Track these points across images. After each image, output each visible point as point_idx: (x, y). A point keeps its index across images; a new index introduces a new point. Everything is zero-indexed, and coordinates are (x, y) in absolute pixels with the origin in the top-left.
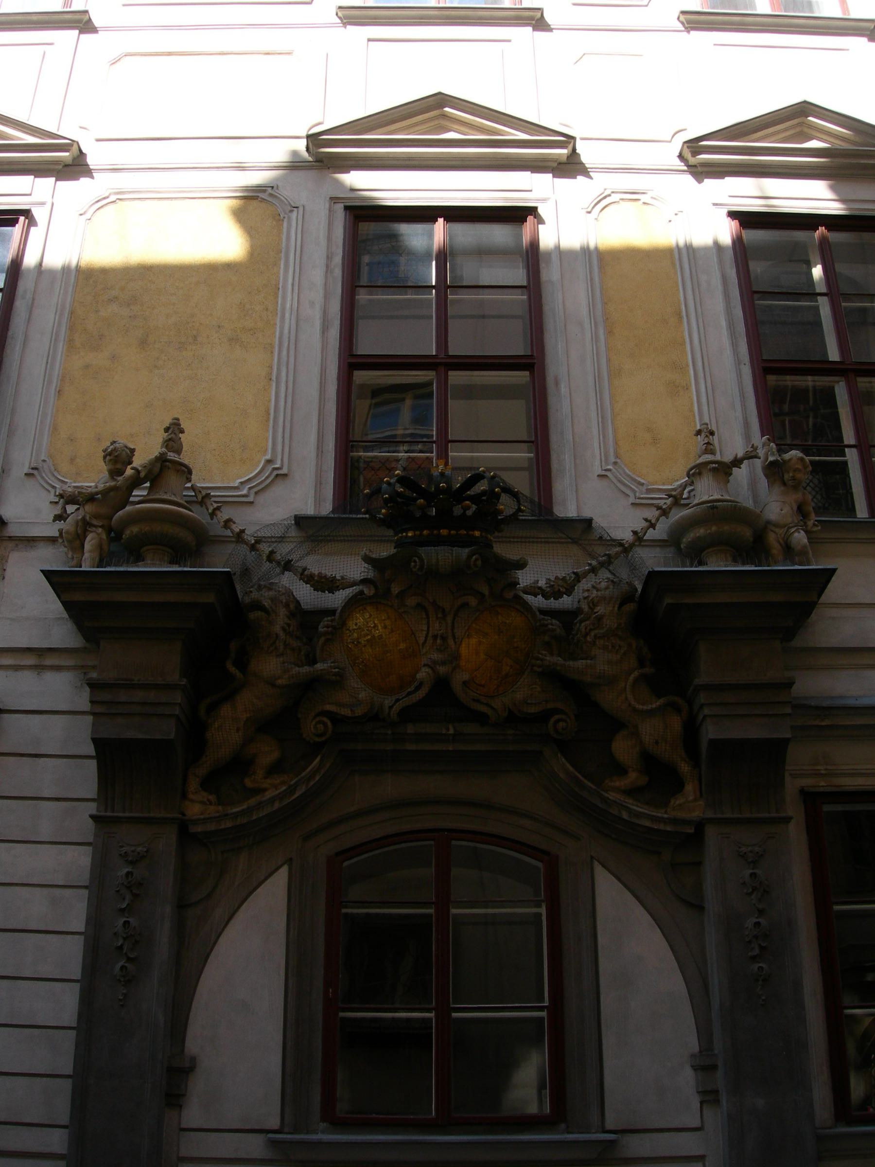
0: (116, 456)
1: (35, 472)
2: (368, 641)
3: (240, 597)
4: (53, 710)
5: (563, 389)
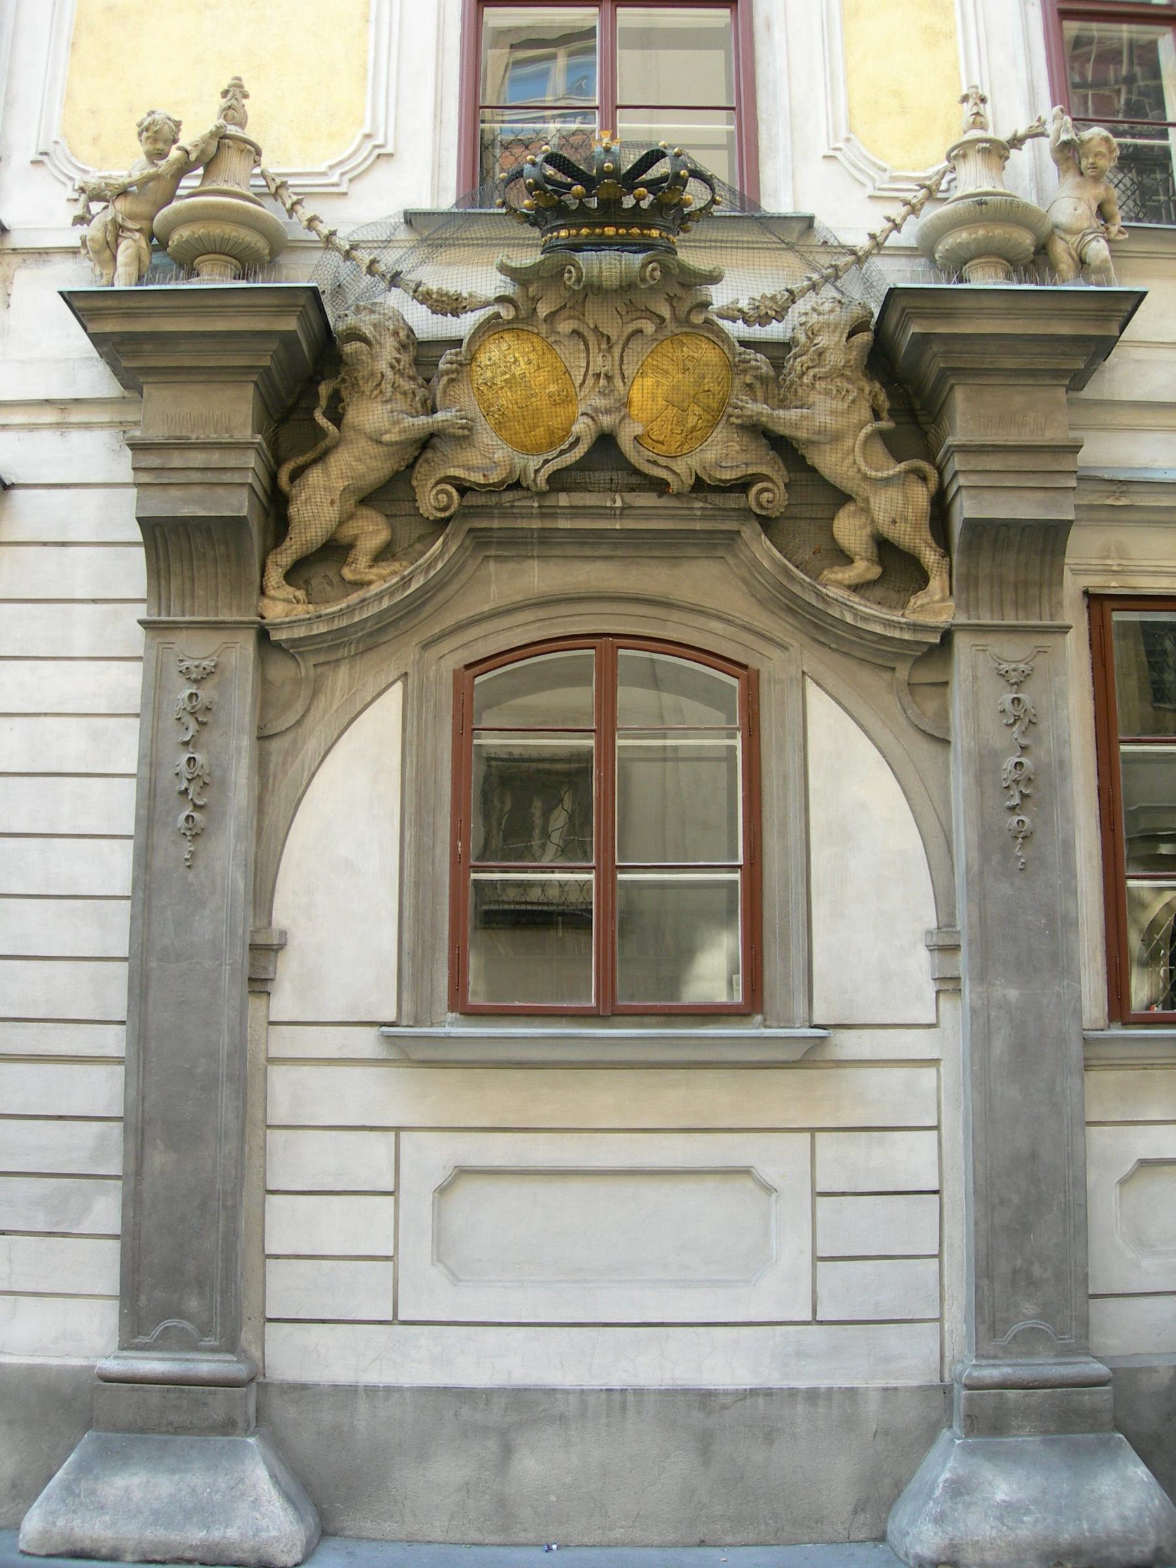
0: (156, 132)
1: (44, 158)
2: (505, 381)
3: (331, 325)
4: (86, 492)
5: (778, 34)
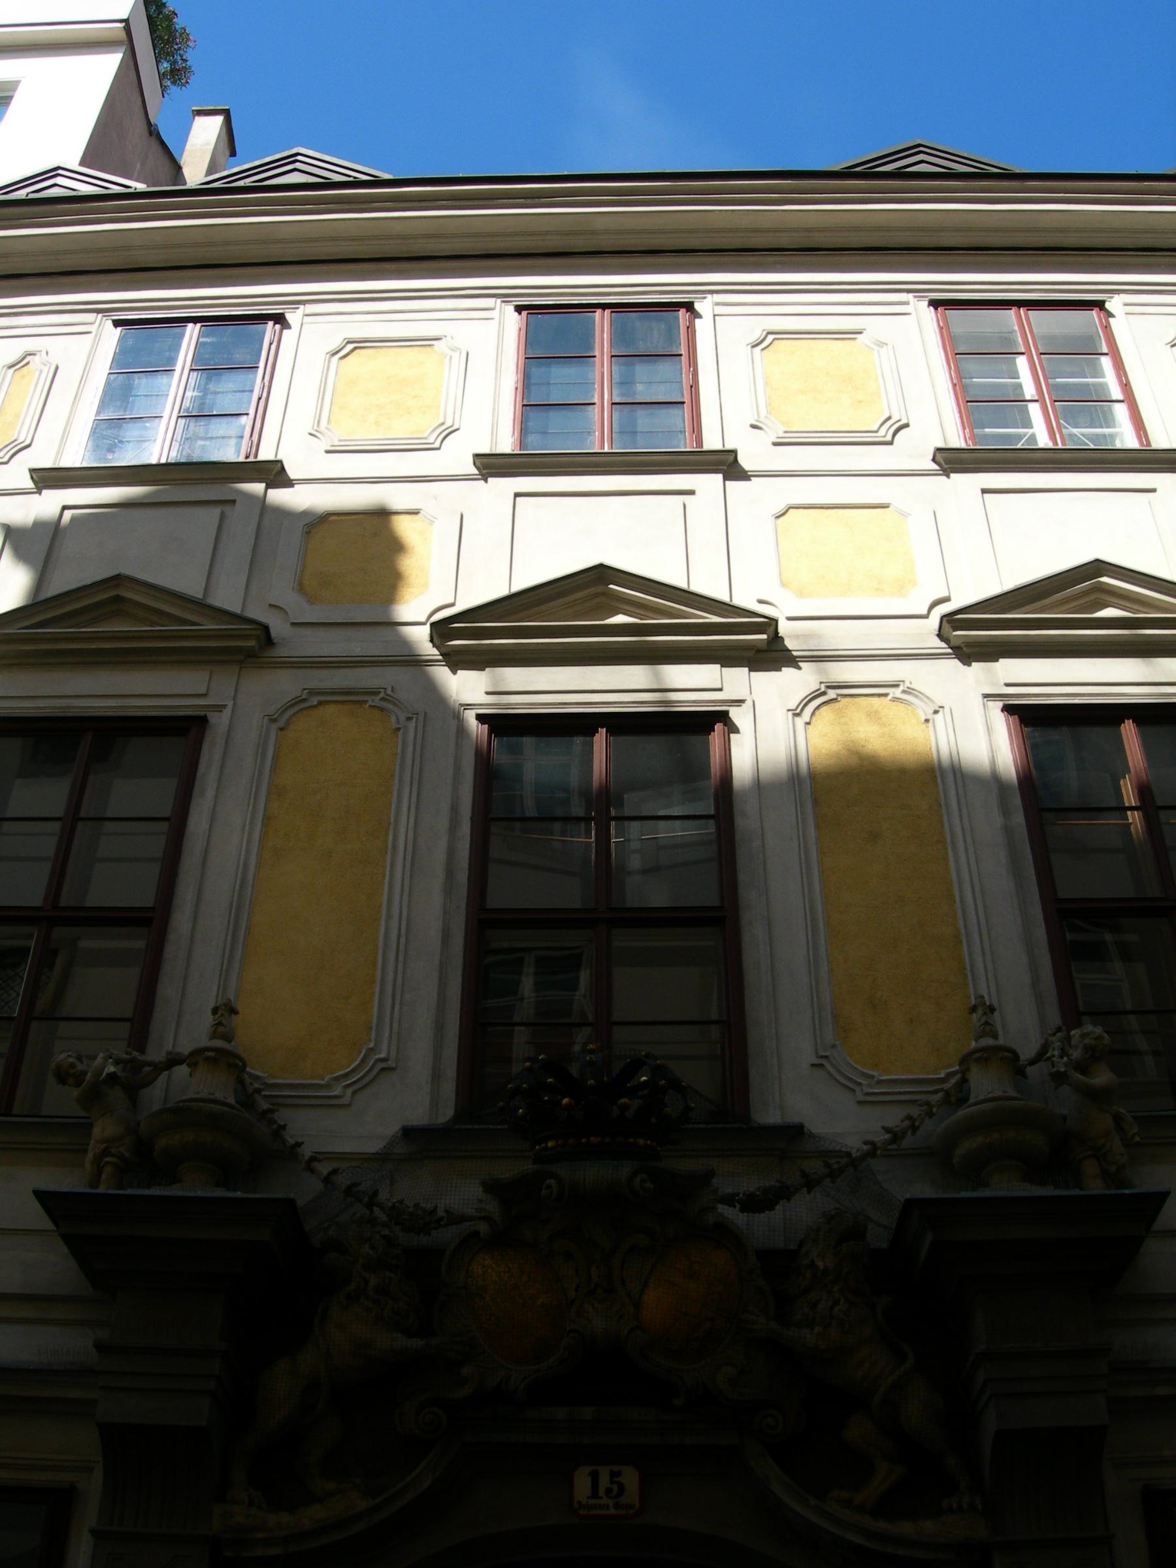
1: (824, 1062)
